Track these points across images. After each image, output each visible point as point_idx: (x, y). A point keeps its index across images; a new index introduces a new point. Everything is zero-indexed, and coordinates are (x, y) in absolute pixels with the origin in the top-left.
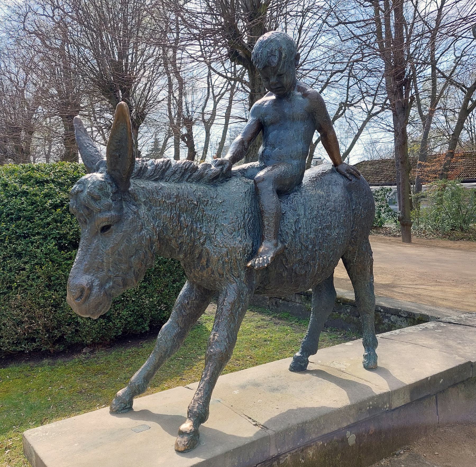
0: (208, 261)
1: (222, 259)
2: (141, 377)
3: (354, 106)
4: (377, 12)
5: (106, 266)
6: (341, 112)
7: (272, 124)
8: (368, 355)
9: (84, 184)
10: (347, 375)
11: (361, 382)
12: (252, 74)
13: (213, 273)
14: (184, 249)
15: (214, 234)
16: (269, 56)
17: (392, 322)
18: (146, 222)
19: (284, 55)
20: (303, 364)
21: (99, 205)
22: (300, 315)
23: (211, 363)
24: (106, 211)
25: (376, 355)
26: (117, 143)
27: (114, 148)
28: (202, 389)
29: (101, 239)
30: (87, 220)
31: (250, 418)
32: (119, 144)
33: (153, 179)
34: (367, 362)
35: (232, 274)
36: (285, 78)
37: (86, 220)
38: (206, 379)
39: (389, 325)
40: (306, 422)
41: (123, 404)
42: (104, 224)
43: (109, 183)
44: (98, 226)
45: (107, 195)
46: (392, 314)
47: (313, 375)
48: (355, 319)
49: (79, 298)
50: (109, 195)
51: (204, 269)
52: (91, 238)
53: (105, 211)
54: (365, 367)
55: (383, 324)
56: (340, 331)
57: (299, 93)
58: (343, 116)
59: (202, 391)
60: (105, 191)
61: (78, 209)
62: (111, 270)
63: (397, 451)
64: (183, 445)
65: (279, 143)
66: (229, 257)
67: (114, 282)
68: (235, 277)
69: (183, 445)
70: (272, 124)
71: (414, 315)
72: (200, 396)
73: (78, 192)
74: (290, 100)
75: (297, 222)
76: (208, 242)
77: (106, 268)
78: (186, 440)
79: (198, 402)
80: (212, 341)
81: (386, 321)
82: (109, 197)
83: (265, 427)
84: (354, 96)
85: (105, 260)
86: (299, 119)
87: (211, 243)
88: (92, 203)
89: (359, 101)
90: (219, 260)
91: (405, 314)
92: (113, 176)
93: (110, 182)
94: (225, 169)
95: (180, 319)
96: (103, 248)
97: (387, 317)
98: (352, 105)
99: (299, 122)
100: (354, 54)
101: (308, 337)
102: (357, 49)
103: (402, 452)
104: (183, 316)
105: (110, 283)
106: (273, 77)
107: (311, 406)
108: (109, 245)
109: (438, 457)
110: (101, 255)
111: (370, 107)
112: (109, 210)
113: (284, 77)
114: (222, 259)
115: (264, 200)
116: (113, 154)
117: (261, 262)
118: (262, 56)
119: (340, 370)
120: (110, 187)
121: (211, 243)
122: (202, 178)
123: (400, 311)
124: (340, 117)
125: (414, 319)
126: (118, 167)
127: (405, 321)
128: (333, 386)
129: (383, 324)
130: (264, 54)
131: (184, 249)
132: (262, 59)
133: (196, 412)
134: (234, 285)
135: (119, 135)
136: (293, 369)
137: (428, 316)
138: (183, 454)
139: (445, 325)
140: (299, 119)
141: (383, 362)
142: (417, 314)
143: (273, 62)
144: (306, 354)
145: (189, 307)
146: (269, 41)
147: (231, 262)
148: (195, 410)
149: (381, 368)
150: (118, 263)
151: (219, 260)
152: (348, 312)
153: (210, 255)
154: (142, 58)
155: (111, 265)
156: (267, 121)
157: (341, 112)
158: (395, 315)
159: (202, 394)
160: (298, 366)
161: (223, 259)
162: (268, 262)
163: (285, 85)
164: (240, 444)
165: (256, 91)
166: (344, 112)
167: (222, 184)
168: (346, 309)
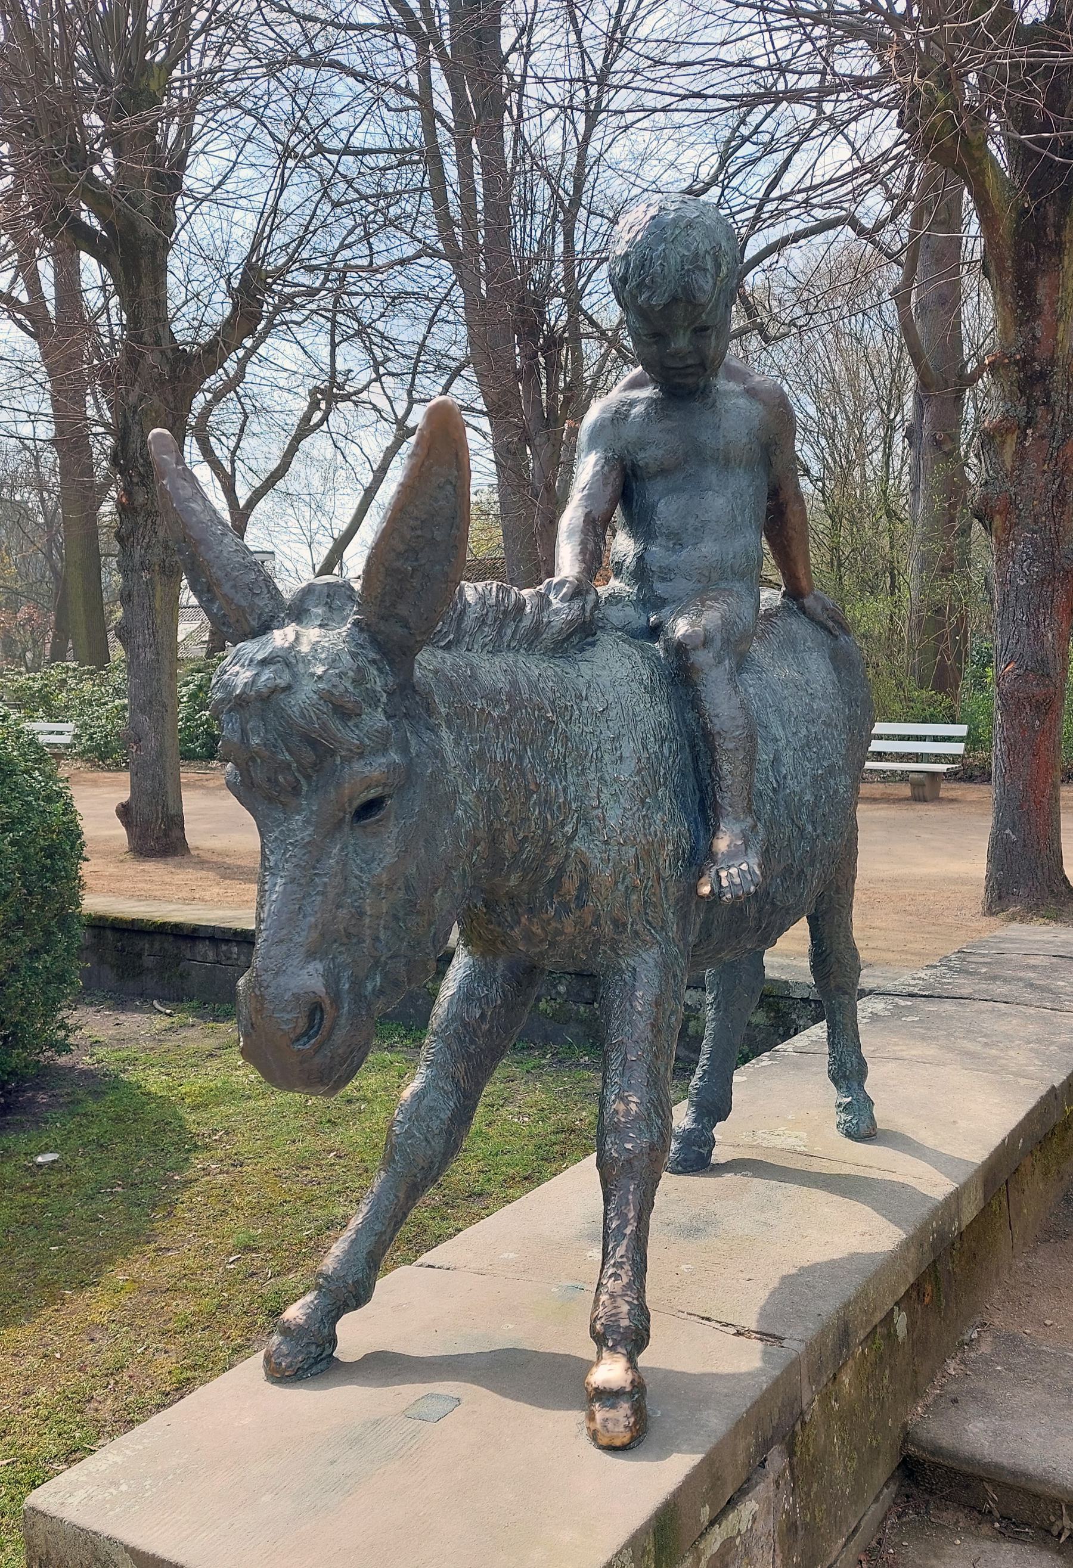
0: (584, 885)
1: (624, 879)
2: (359, 1255)
3: (354, 402)
4: (430, 133)
5: (369, 927)
6: (317, 416)
7: (663, 472)
8: (854, 1102)
9: (288, 664)
10: (825, 1163)
11: (876, 1175)
12: (130, 285)
13: (597, 922)
14: (524, 857)
15: (598, 808)
16: (689, 270)
18: (460, 780)
19: (724, 269)
20: (704, 1151)
21: (357, 732)
22: (411, 1017)
23: (631, 1182)
24: (378, 751)
25: (868, 1099)
26: (413, 529)
27: (401, 548)
28: (624, 1260)
29: (353, 842)
30: (303, 782)
31: (708, 1319)
32: (419, 532)
33: (443, 644)
34: (854, 1122)
35: (648, 921)
36: (713, 338)
37: (298, 781)
38: (628, 1231)
40: (850, 1303)
41: (314, 1346)
42: (372, 794)
43: (373, 662)
44: (350, 801)
45: (375, 702)
47: (746, 1175)
48: (582, 1009)
49: (305, 1034)
50: (379, 700)
51: (568, 911)
52: (322, 841)
53: (375, 752)
54: (848, 1135)
56: (541, 1048)
57: (732, 386)
58: (324, 427)
59: (627, 1267)
60: (368, 686)
61: (275, 746)
62: (382, 937)
63: (963, 1334)
64: (626, 1427)
65: (696, 529)
66: (642, 871)
67: (385, 976)
68: (654, 928)
69: (626, 1427)
70: (663, 472)
72: (625, 1280)
73: (275, 690)
74: (713, 405)
75: (776, 760)
76: (583, 831)
77: (368, 932)
78: (629, 1412)
79: (627, 1298)
80: (623, 1120)
82: (377, 707)
83: (766, 1335)
84: (350, 371)
85: (368, 908)
86: (741, 461)
87: (592, 833)
88: (335, 725)
89: (366, 387)
90: (616, 883)
92: (379, 638)
93: (372, 655)
94: (588, 608)
95: (461, 1066)
96: (361, 870)
98: (347, 397)
99: (742, 471)
100: (343, 246)
101: (710, 1074)
102: (351, 232)
103: (975, 1335)
104: (470, 1056)
105: (374, 979)
106: (682, 332)
108: (381, 860)
109: (1056, 1330)
110: (355, 892)
111: (400, 409)
112: (384, 750)
113: (710, 337)
114: (624, 879)
115: (716, 701)
116: (398, 564)
117: (737, 880)
118: (666, 269)
119: (795, 1152)
120: (375, 673)
121: (592, 833)
122: (537, 638)
124: (313, 431)
126: (403, 610)
128: (819, 1195)
130: (672, 262)
131: (524, 857)
132: (664, 278)
133: (627, 1327)
134: (655, 950)
135: (423, 503)
136: (680, 1168)
137: (786, 982)
138: (630, 1453)
139: (909, 1003)
140: (741, 461)
143: (700, 288)
144: (709, 1121)
145: (485, 1027)
146: (682, 225)
147: (646, 887)
148: (625, 1323)
149: (885, 1132)
150: (401, 914)
151: (616, 883)
152: (559, 993)
153: (591, 871)
155: (382, 922)
156: (647, 464)
157: (317, 416)
158: (695, 988)
159: (630, 1273)
160: (692, 1156)
161: (628, 880)
162: (756, 880)
163: (710, 358)
164: (754, 1394)
165: (147, 338)
166: (325, 419)
167: (587, 654)
168: (555, 987)
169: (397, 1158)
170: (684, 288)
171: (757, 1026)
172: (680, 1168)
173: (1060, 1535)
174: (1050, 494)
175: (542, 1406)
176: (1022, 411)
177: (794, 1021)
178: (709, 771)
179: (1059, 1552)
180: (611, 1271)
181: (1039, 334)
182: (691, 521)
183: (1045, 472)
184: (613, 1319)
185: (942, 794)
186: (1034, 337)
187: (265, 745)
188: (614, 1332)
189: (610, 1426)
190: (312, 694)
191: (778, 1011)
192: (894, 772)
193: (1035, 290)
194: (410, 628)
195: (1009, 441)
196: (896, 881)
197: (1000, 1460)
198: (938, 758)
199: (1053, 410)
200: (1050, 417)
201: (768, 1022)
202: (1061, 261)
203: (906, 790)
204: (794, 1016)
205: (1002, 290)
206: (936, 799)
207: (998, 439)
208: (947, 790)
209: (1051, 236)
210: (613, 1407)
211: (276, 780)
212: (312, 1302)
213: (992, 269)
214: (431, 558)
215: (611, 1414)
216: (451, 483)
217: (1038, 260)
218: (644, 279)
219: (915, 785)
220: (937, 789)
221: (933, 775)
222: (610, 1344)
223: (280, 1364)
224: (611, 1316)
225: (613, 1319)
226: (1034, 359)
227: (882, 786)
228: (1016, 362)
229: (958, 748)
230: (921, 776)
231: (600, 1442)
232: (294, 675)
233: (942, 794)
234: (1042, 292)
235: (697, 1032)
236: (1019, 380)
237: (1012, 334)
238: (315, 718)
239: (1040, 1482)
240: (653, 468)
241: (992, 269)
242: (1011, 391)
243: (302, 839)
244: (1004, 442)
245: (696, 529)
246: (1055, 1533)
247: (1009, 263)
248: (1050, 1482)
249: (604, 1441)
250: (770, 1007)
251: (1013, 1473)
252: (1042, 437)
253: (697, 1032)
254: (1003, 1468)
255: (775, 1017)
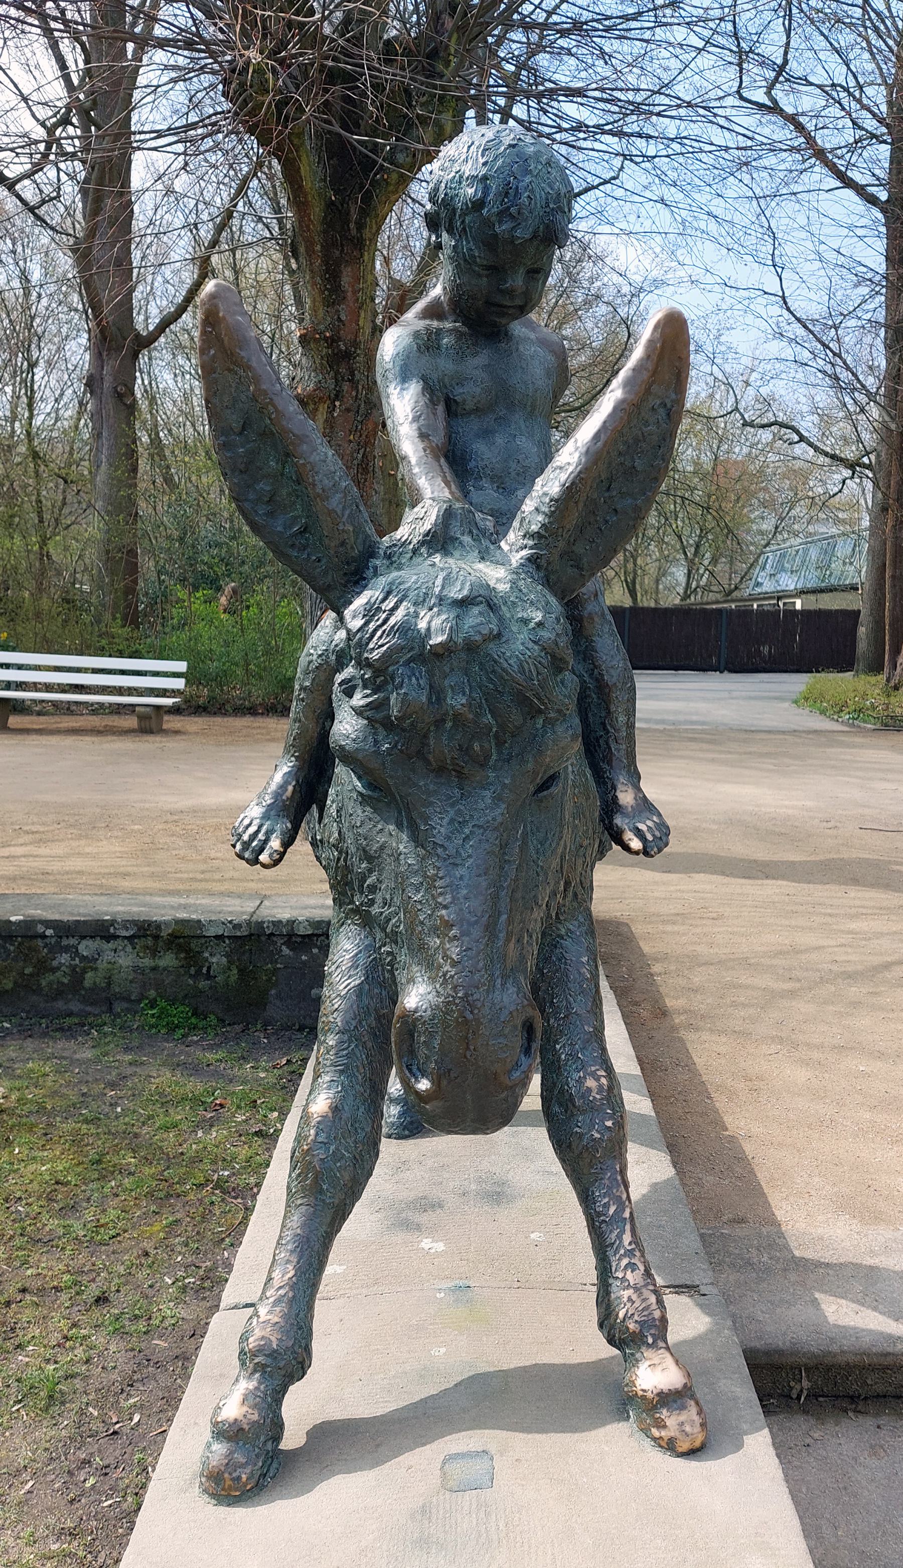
16: (553, 209)
17: (84, 958)
39: (74, 970)
46: (83, 937)
55: (54, 970)
70: (478, 411)
71: (158, 926)
80: (598, 1097)
81: (64, 958)
91: (127, 929)
97: (66, 949)
107: (594, 1359)
123: (112, 922)
125: (156, 937)
127: (129, 949)
129: (54, 970)
136: (407, 1132)
137: (199, 921)
141: (601, 908)
142: (166, 923)
154: (203, 55)
158: (92, 937)
169: (325, 1187)
170: (547, 227)
171: (165, 969)
172: (407, 1132)
173: (799, 1398)
174: (355, 462)
175: (574, 1429)
176: (331, 384)
177: (206, 960)
178: (604, 724)
179: (806, 1412)
180: (625, 1261)
181: (343, 318)
182: (513, 465)
183: (350, 441)
184: (645, 1313)
185: (165, 727)
186: (339, 320)
187: (470, 705)
188: (650, 1327)
189: (688, 1429)
190: (531, 645)
191: (188, 951)
192: (101, 705)
193: (340, 277)
194: (582, 569)
195: (321, 409)
196: (195, 811)
197: (753, 1344)
198: (163, 693)
199: (357, 387)
200: (354, 393)
201: (176, 963)
202: (362, 256)
203: (131, 722)
204: (206, 955)
205: (312, 271)
206: (161, 731)
207: (312, 406)
208: (171, 722)
209: (354, 232)
210: (683, 1408)
211: (470, 747)
212: (257, 1388)
213: (302, 250)
214: (624, 490)
215: (683, 1417)
216: (665, 405)
217: (342, 250)
218: (509, 208)
219: (142, 718)
220: (161, 722)
221: (158, 708)
222: (650, 1341)
223: (239, 1478)
224: (643, 1310)
225: (645, 1313)
226: (340, 339)
227: (90, 718)
228: (326, 339)
229: (179, 684)
230: (148, 709)
231: (680, 1450)
232: (501, 619)
233: (165, 727)
234: (346, 280)
235: (95, 983)
236: (328, 355)
237: (321, 313)
238: (535, 674)
239: (792, 1354)
240: (470, 405)
241: (302, 250)
242: (321, 364)
243: (494, 819)
244: (317, 410)
245: (518, 474)
246: (794, 1396)
247: (318, 248)
248: (799, 1352)
249: (684, 1446)
250: (180, 948)
251: (767, 1353)
252: (348, 410)
253: (95, 983)
254: (758, 1350)
255: (186, 958)
